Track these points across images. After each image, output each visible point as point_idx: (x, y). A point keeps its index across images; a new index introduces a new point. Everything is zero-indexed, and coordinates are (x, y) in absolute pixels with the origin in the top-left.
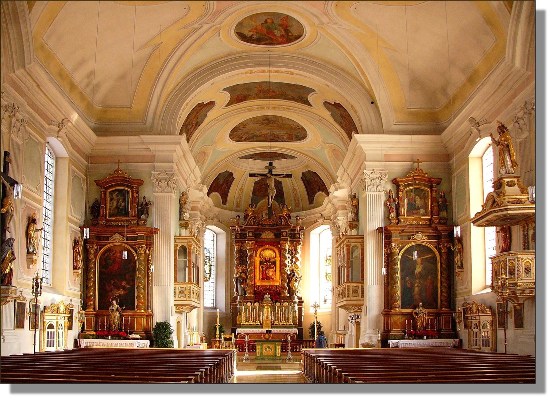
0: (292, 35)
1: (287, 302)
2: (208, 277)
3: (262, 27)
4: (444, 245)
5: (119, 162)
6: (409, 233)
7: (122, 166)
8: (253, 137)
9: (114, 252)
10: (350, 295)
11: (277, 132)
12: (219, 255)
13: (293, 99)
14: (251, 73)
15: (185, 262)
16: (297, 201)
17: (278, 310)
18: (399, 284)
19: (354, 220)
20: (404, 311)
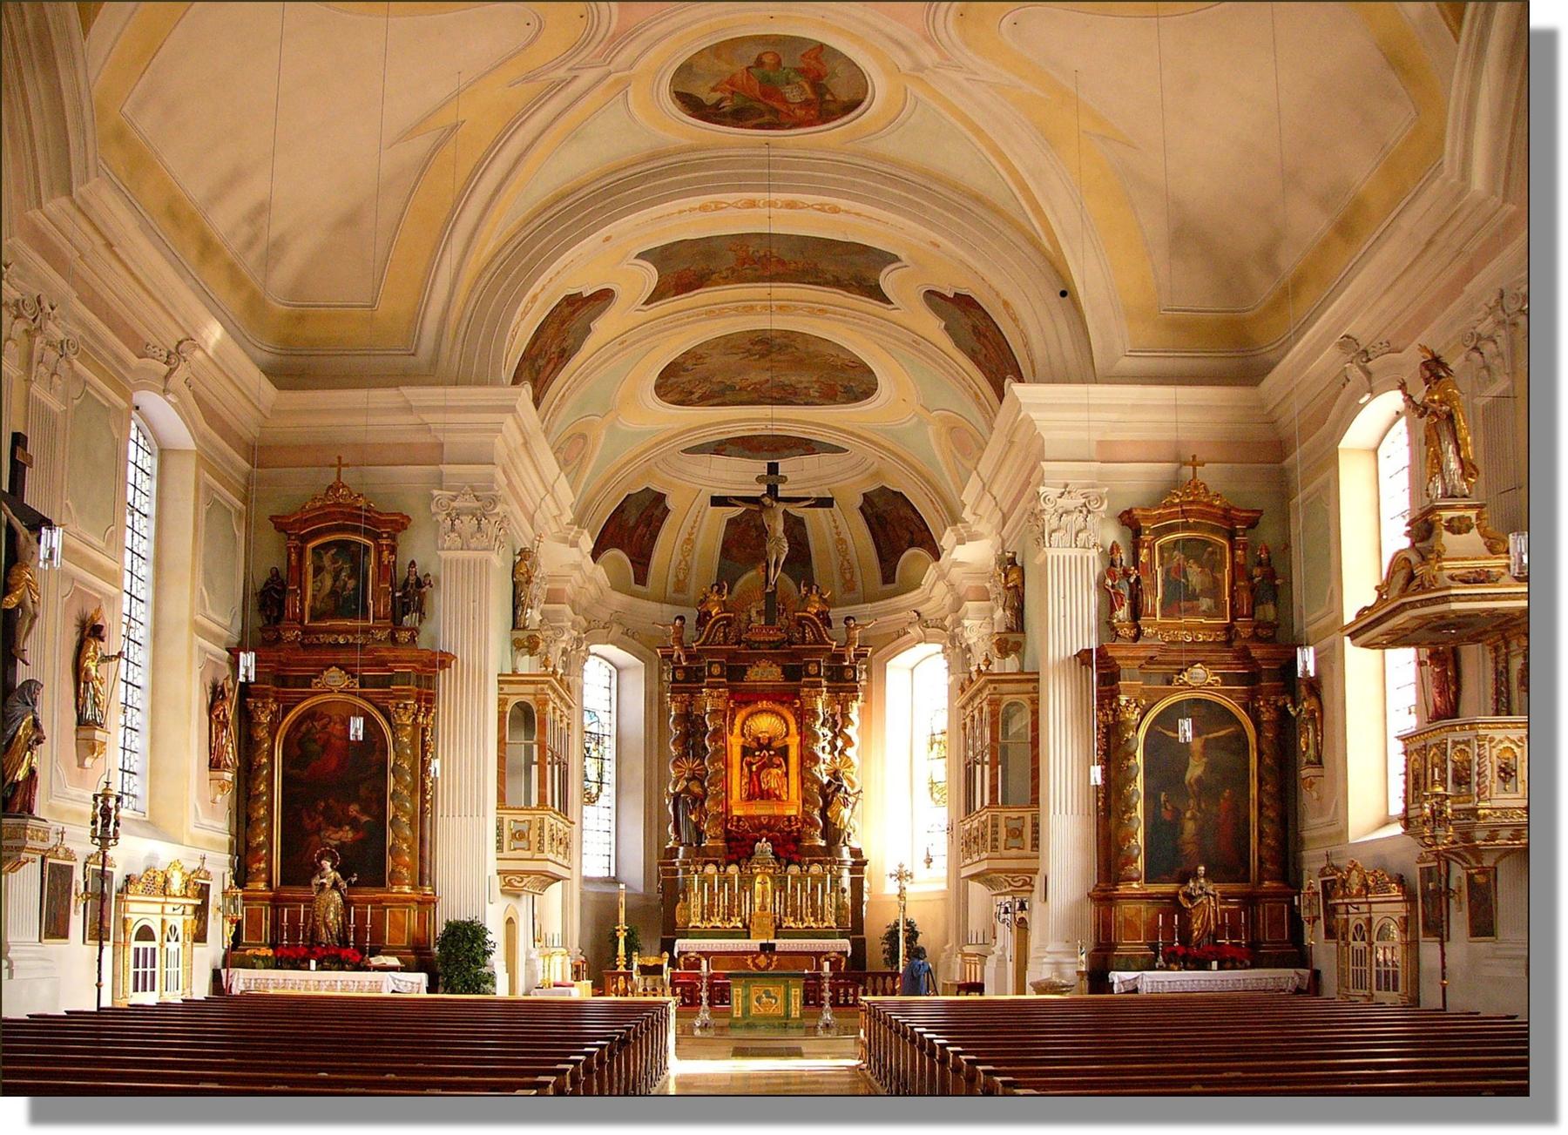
0: (835, 101)
1: (820, 862)
2: (594, 791)
3: (748, 78)
4: (1267, 702)
5: (340, 464)
6: (1168, 666)
7: (348, 476)
8: (722, 393)
9: (325, 721)
10: (1001, 844)
11: (791, 378)
12: (625, 730)
13: (837, 283)
14: (717, 209)
15: (529, 750)
16: (848, 576)
17: (794, 887)
18: (1139, 813)
19: (1010, 630)
20: (1153, 889)
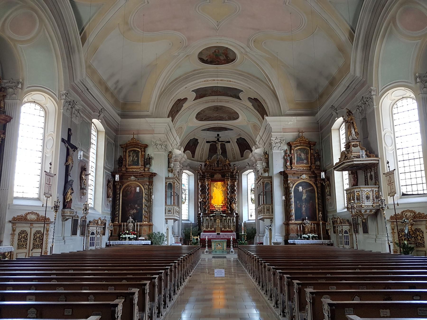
5: (134, 134)
6: (298, 174)
8: (209, 118)
10: (265, 212)
13: (231, 96)
15: (171, 193)
17: (224, 221)
18: (293, 206)
19: (266, 167)
20: (297, 222)
